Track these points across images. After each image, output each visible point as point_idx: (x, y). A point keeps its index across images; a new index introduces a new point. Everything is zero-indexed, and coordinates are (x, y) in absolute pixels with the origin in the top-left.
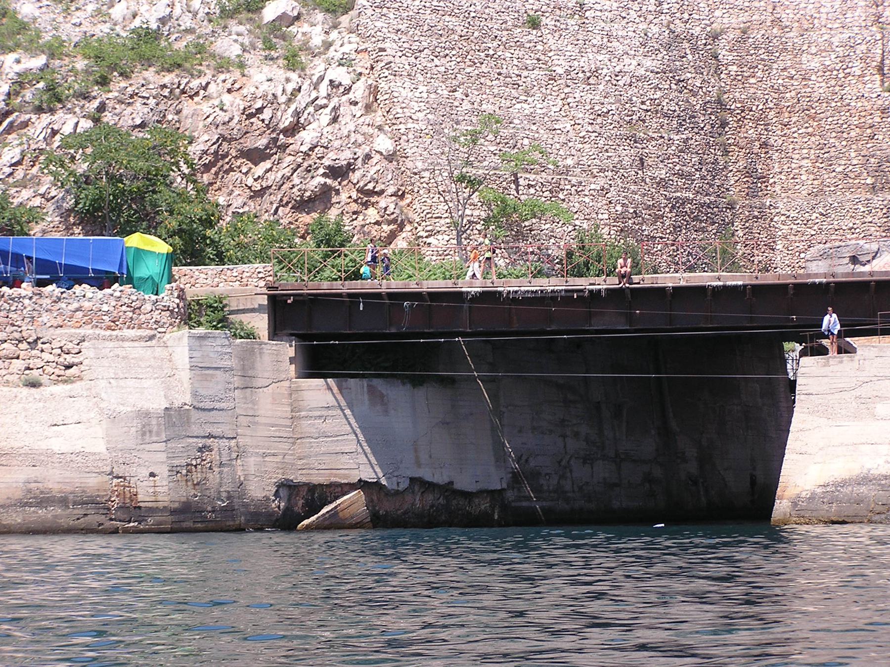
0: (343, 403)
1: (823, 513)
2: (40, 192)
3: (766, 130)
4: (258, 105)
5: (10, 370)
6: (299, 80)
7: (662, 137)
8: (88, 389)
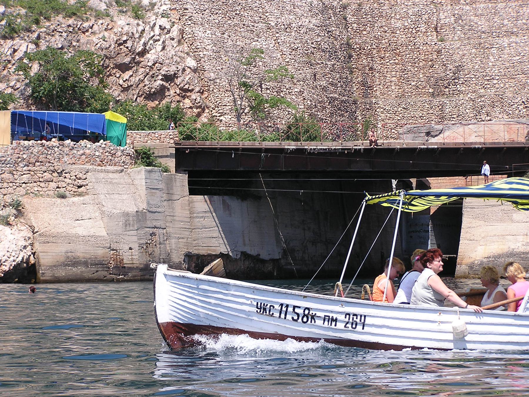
0: (212, 210)
2: (10, 85)
3: (372, 60)
4: (125, 38)
5: (49, 188)
6: (143, 25)
7: (322, 63)
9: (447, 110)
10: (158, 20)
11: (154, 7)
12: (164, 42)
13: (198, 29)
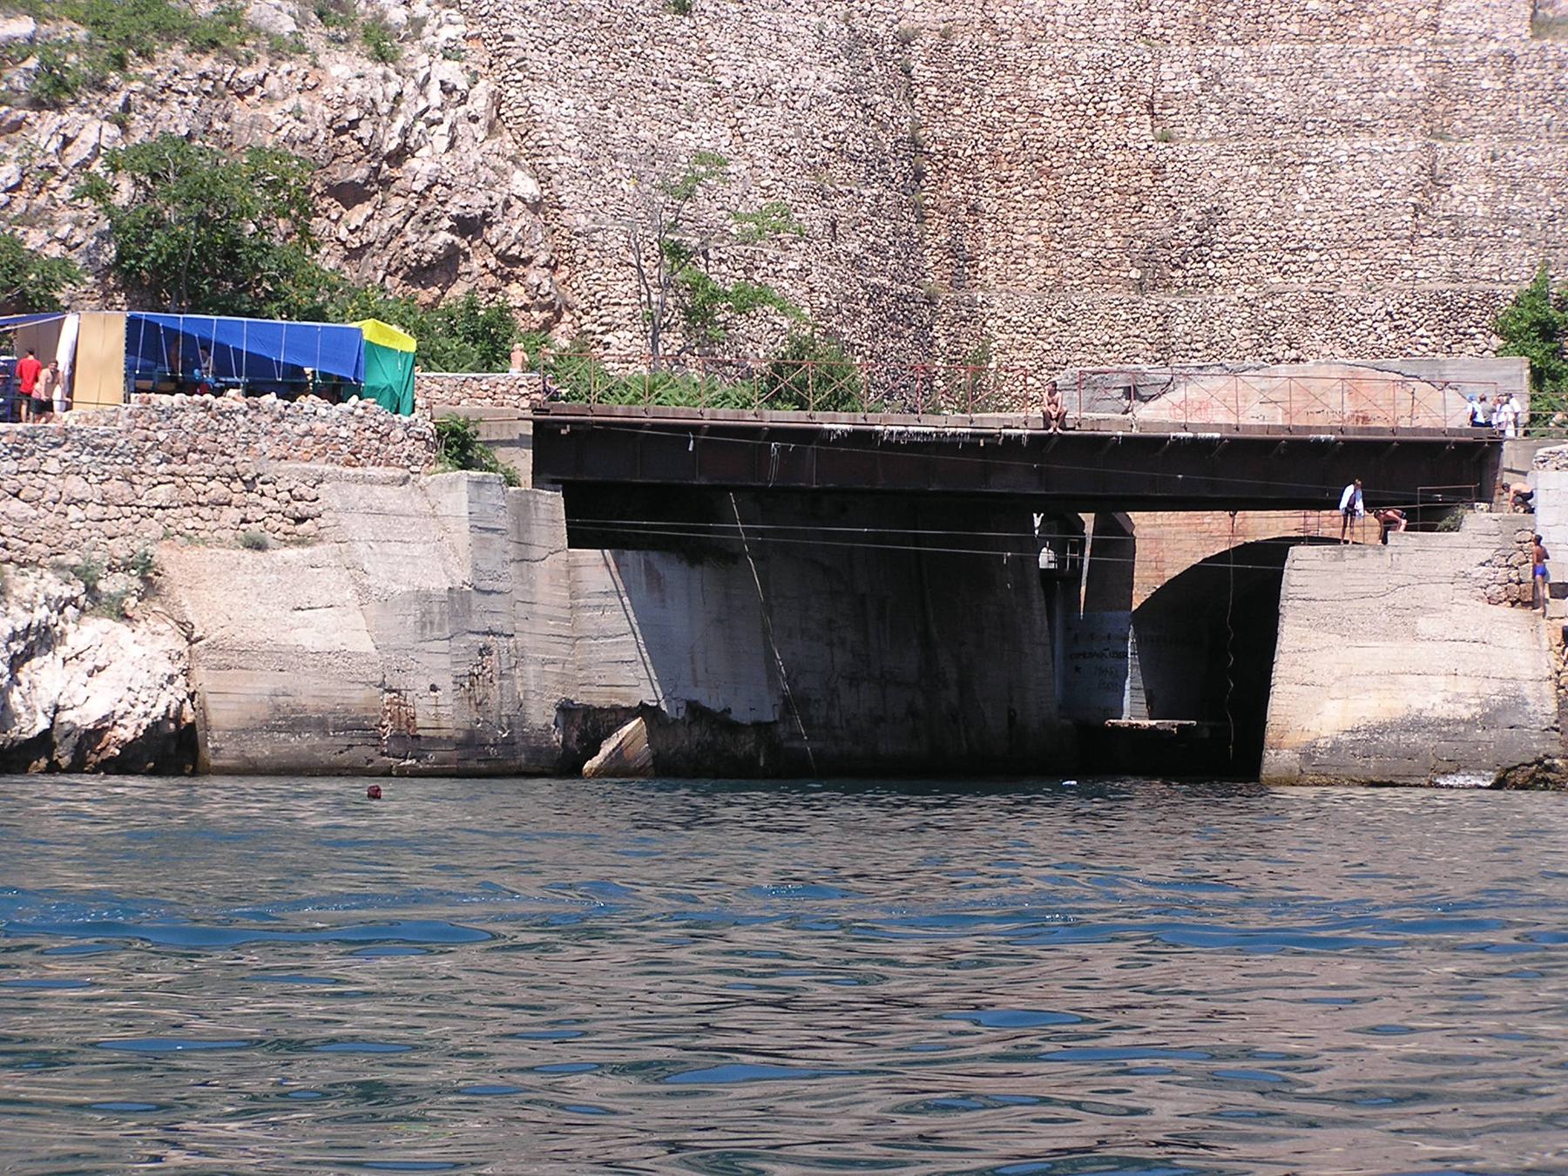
0: (622, 588)
1: (1355, 770)
2: (58, 235)
3: (976, 187)
4: (353, 114)
5: (222, 523)
6: (399, 78)
7: (851, 192)
8: (335, 556)
9: (1180, 328)
10: (434, 64)
11: (421, 31)
12: (452, 127)
13: (542, 94)
